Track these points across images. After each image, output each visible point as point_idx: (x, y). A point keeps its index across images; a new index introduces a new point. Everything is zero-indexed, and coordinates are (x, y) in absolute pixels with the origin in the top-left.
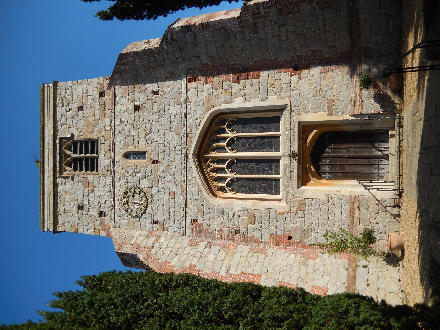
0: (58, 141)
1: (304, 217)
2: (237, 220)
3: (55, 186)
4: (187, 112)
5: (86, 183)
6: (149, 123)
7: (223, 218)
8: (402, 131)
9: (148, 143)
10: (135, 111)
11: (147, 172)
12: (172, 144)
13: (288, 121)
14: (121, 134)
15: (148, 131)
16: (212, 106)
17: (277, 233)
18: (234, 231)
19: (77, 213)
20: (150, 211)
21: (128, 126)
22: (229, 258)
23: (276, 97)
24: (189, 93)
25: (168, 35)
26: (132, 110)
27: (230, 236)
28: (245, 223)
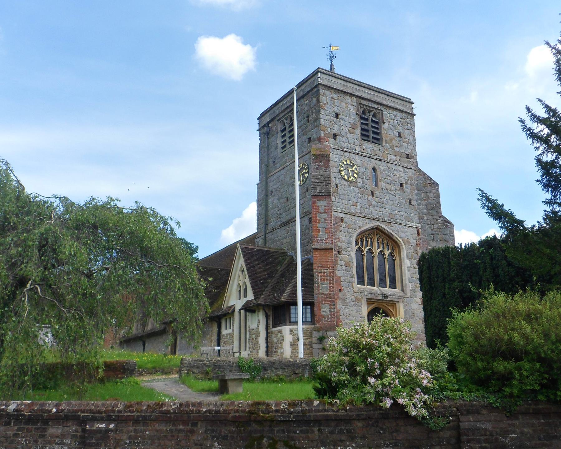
0: (380, 107)
3: (352, 95)
5: (354, 127)
12: (383, 210)
14: (387, 168)
18: (340, 250)
21: (392, 176)
22: (503, 307)
24: (411, 228)
28: (345, 259)
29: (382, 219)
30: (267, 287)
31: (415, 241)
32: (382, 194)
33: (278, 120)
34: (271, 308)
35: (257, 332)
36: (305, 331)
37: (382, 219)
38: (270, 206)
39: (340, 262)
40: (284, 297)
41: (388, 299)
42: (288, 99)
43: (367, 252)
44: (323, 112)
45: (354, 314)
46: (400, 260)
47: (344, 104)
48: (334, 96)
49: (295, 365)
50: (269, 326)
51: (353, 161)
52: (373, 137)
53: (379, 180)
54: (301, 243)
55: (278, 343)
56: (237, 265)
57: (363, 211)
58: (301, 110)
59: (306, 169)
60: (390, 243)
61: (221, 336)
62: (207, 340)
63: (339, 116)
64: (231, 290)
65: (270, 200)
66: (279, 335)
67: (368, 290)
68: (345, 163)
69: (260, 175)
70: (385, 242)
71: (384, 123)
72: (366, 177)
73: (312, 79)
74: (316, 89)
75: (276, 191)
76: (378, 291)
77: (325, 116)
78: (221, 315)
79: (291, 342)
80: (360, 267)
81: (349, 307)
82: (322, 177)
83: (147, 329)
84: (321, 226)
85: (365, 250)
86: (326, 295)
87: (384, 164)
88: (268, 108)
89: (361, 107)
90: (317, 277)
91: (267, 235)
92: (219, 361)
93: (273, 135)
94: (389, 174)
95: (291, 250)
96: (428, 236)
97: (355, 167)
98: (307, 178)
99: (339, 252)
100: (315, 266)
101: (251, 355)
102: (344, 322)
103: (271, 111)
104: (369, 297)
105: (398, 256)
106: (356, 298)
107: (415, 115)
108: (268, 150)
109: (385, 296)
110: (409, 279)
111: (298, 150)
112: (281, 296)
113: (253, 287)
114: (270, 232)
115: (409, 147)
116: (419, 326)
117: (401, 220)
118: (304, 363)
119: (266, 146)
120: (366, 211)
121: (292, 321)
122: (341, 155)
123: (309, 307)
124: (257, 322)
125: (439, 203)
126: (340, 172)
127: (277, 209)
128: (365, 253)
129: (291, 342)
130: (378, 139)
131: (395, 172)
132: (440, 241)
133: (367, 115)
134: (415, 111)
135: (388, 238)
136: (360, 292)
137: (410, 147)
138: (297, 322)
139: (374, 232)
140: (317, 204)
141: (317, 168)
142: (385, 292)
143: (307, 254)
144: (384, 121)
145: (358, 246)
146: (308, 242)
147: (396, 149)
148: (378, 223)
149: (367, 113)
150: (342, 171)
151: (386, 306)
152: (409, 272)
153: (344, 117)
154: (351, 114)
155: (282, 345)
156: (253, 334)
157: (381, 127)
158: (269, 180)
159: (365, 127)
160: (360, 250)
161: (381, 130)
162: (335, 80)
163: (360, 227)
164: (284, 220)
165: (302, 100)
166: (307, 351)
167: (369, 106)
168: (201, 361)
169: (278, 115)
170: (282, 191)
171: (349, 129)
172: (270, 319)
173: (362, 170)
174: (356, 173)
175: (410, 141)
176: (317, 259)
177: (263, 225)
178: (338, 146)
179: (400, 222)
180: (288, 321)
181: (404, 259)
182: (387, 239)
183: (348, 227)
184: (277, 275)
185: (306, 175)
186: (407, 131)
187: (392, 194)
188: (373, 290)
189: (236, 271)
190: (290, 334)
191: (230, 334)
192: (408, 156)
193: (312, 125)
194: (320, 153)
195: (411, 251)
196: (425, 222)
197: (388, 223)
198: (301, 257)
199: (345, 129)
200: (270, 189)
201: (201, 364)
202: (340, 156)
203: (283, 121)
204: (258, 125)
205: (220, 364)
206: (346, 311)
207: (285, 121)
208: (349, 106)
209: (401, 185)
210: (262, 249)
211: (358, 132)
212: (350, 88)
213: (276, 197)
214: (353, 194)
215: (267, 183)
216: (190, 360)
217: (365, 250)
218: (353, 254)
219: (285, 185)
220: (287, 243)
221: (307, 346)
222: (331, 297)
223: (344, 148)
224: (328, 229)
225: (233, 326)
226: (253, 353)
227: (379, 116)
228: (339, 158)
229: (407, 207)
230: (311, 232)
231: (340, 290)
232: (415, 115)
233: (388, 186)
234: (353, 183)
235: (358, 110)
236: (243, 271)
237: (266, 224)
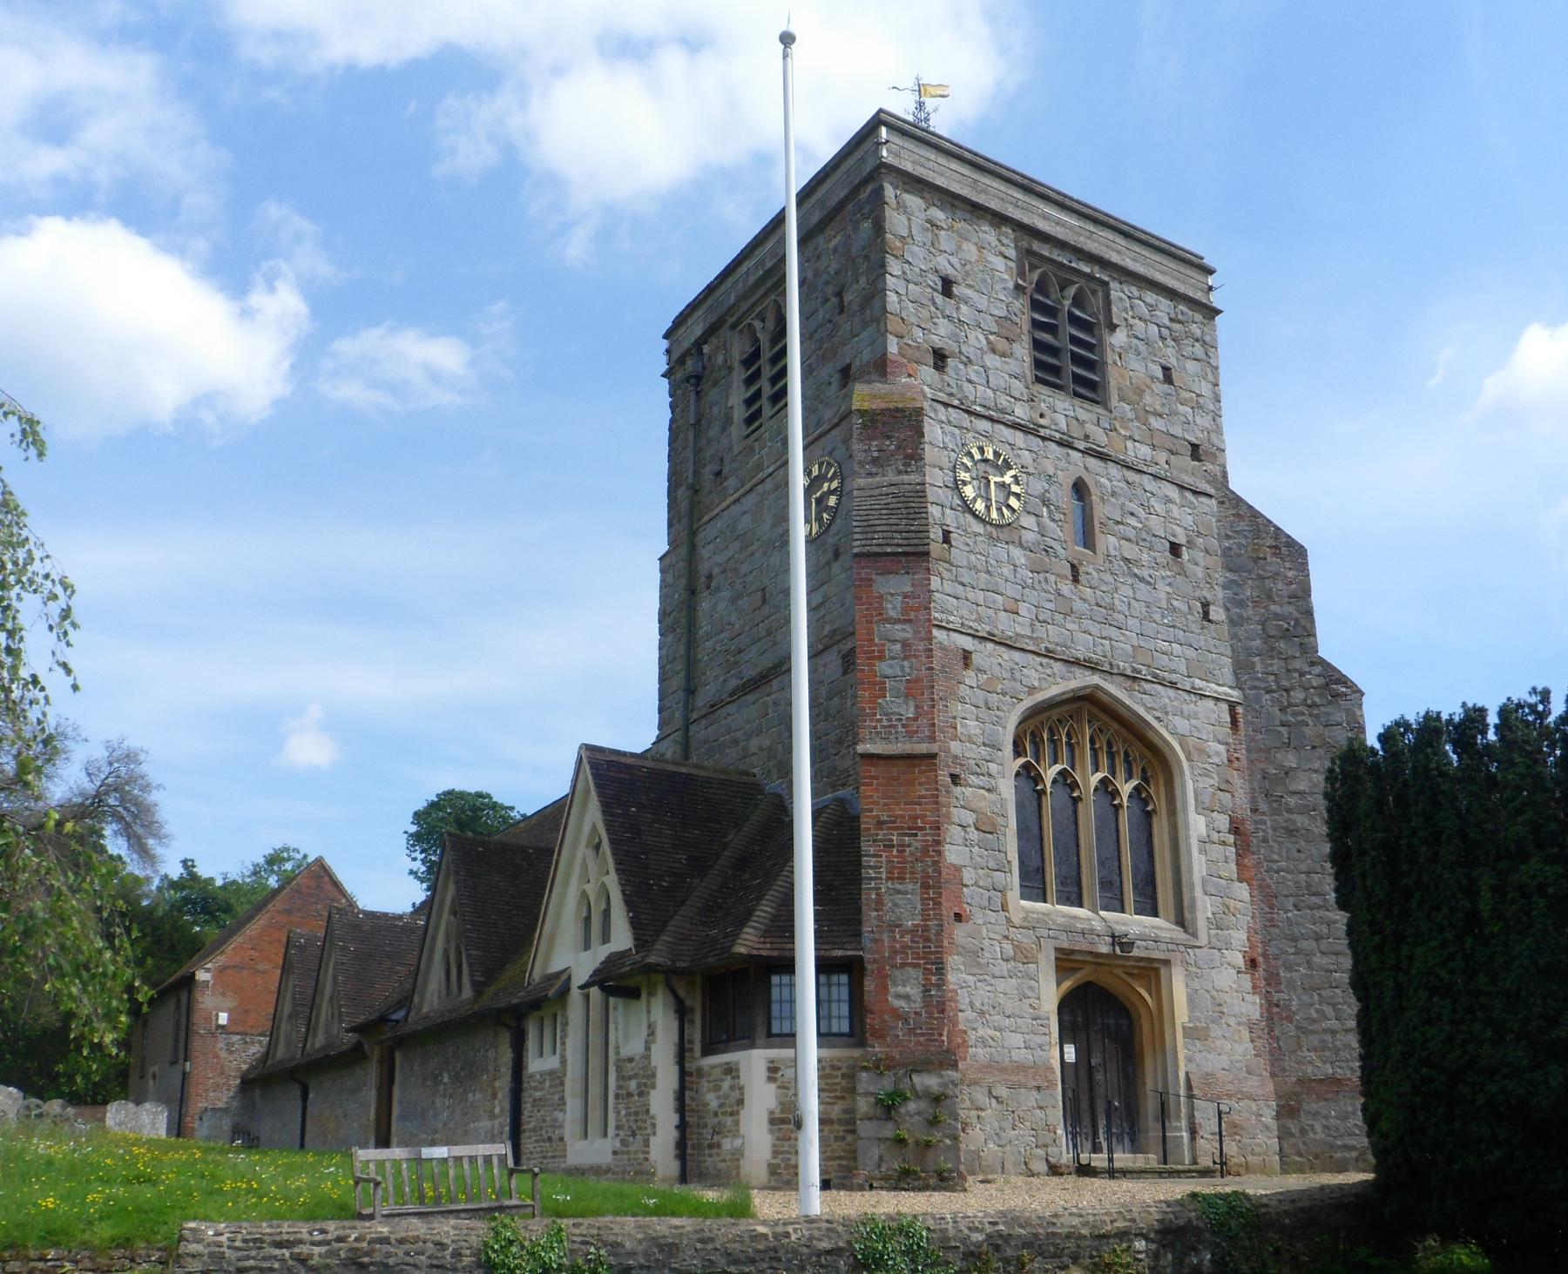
1: (1003, 959)
2: (981, 784)
4: (1178, 689)
6: (1151, 577)
7: (982, 704)
8: (1193, 1177)
9: (1111, 562)
10: (1170, 542)
11: (1054, 544)
12: (1113, 632)
13: (1172, 939)
14: (1123, 485)
15: (1136, 570)
16: (1189, 759)
17: (966, 886)
18: (957, 771)
19: (937, 271)
20: (970, 527)
21: (1141, 512)
23: (1210, 915)
24: (1211, 703)
25: (1347, 688)
26: (1174, 536)
27: (945, 756)
28: (981, 805)
29: (1111, 664)
30: (683, 903)
31: (1222, 748)
32: (1108, 577)
33: (733, 327)
34: (698, 979)
35: (645, 1068)
36: (826, 1071)
37: (1111, 664)
38: (705, 627)
39: (959, 814)
40: (748, 942)
41: (1135, 953)
42: (770, 244)
43: (1054, 781)
44: (894, 266)
45: (1009, 1006)
46: (1172, 813)
47: (974, 249)
48: (938, 214)
49: (781, 1254)
50: (691, 1050)
51: (1005, 451)
52: (1074, 374)
53: (1097, 525)
54: (812, 747)
55: (725, 1114)
56: (579, 829)
57: (1041, 631)
58: (816, 275)
59: (832, 479)
60: (1135, 754)
61: (525, 1079)
62: (481, 1090)
63: (955, 290)
64: (558, 915)
65: (705, 606)
66: (727, 1084)
67: (1060, 920)
68: (977, 456)
69: (670, 526)
70: (1119, 748)
71: (1113, 327)
72: (1050, 512)
73: (857, 155)
74: (870, 188)
75: (724, 571)
76: (1098, 925)
78: (520, 1005)
79: (772, 1113)
80: (1030, 834)
82: (892, 490)
83: (313, 1045)
84: (889, 671)
85: (1050, 773)
86: (907, 932)
87: (1114, 470)
88: (699, 295)
89: (1033, 267)
90: (875, 862)
91: (693, 728)
92: (385, 1241)
93: (715, 384)
94: (1133, 506)
95: (775, 776)
96: (1268, 731)
97: (1012, 472)
98: (834, 511)
99: (955, 779)
100: (866, 822)
101: (622, 1153)
102: (972, 1035)
103: (709, 301)
104: (1065, 945)
105: (1163, 804)
107: (1218, 312)
108: (697, 437)
109: (1120, 941)
110: (1204, 882)
111: (805, 419)
112: (735, 935)
113: (629, 903)
114: (703, 717)
115: (1198, 420)
116: (1240, 1049)
117: (1174, 671)
118: (825, 1245)
119: (692, 421)
120: (1052, 635)
121: (775, 1029)
122: (960, 428)
123: (844, 978)
124: (644, 1033)
125: (1309, 613)
126: (957, 486)
127: (726, 634)
128: (1048, 784)
129: (772, 1113)
130: (1092, 385)
131: (1153, 501)
132: (1314, 748)
133: (1053, 297)
134: (1215, 300)
135: (1130, 737)
136: (1030, 925)
137: (1203, 421)
138: (793, 1035)
139: (1079, 711)
140: (875, 587)
141: (875, 461)
142: (1119, 929)
143: (834, 787)
144: (1115, 321)
145: (1021, 761)
146: (840, 742)
148: (1096, 679)
149: (1054, 290)
150: (965, 483)
151: (1125, 977)
153: (970, 293)
154: (998, 287)
155: (737, 1123)
156: (630, 1078)
157: (1100, 340)
158: (700, 536)
159: (1046, 337)
160: (1029, 775)
161: (1102, 354)
162: (942, 160)
163: (1032, 690)
164: (750, 672)
165: (820, 239)
166: (835, 1146)
167: (1061, 265)
168: (280, 1245)
169: (731, 310)
170: (744, 569)
171: (992, 337)
172: (692, 1022)
173: (1038, 486)
174: (1018, 496)
175: (1201, 400)
176: (873, 804)
177: (680, 695)
178: (951, 395)
179: (1174, 677)
180: (761, 1030)
181: (1185, 810)
182: (1125, 741)
184: (721, 862)
185: (832, 501)
186: (1191, 366)
187: (1142, 580)
188: (1075, 918)
189: (575, 848)
190: (771, 1079)
191: (551, 1073)
192: (1195, 451)
193: (856, 320)
194: (884, 406)
195: (1212, 782)
196: (1257, 683)
197: (1129, 683)
198: (815, 794)
199: (977, 339)
200: (704, 568)
201: (283, 1260)
202: (957, 431)
203: (750, 325)
204: (664, 359)
205: (388, 1255)
206: (982, 995)
207: (757, 324)
208: (992, 258)
209: (1175, 549)
210: (671, 768)
211: (1023, 350)
212: (994, 195)
213: (726, 594)
214: (1007, 571)
215: (693, 548)
216: (223, 1239)
217: (1050, 773)
218: (1007, 788)
219: (755, 547)
220: (761, 749)
221: (837, 1127)
222: (927, 940)
223: (975, 403)
224: (917, 680)
225: (563, 1043)
226: (632, 1149)
227: (1097, 302)
228: (953, 435)
229: (1193, 627)
230: (849, 703)
231: (958, 917)
232: (1218, 312)
233: (1130, 551)
234: (1004, 531)
235: (1021, 274)
236: (597, 847)
237: (690, 691)
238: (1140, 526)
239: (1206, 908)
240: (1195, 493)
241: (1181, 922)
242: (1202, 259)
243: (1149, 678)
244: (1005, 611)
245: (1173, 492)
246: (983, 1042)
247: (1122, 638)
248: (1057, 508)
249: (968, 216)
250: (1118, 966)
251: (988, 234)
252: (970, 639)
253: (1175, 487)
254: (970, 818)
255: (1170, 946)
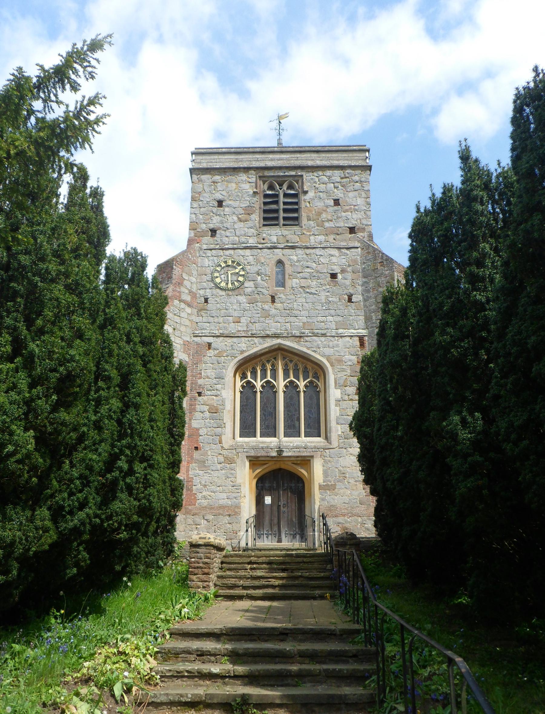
3: (246, 170)
7: (216, 362)
12: (292, 319)
14: (305, 256)
15: (308, 290)
16: (332, 365)
17: (201, 436)
18: (201, 390)
24: (348, 339)
28: (210, 402)
48: (217, 178)
51: (237, 259)
70: (300, 367)
77: (198, 209)
81: (212, 472)
87: (299, 251)
94: (309, 264)
104: (252, 454)
106: (226, 458)
110: (337, 419)
120: (256, 328)
131: (321, 259)
135: (305, 361)
139: (277, 354)
147: (327, 225)
148: (279, 341)
152: (338, 408)
153: (230, 202)
162: (221, 157)
183: (219, 355)
197: (298, 339)
206: (206, 478)
209: (334, 276)
217: (258, 384)
238: (313, 271)
239: (338, 430)
240: (348, 248)
241: (327, 438)
242: (365, 146)
243: (310, 334)
244: (234, 322)
245: (335, 252)
246: (205, 498)
247: (297, 320)
248: (266, 275)
249: (232, 173)
250: (288, 461)
251: (243, 177)
252: (212, 338)
253: (335, 249)
254: (206, 408)
255: (313, 450)
